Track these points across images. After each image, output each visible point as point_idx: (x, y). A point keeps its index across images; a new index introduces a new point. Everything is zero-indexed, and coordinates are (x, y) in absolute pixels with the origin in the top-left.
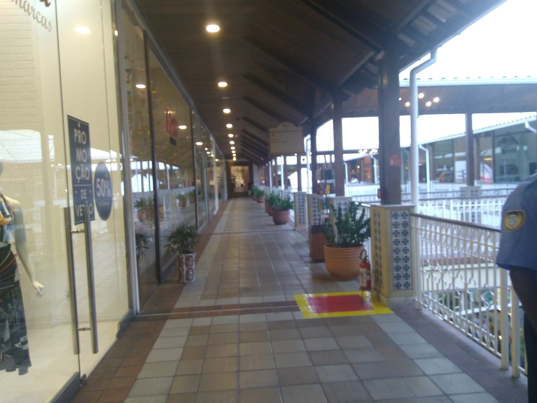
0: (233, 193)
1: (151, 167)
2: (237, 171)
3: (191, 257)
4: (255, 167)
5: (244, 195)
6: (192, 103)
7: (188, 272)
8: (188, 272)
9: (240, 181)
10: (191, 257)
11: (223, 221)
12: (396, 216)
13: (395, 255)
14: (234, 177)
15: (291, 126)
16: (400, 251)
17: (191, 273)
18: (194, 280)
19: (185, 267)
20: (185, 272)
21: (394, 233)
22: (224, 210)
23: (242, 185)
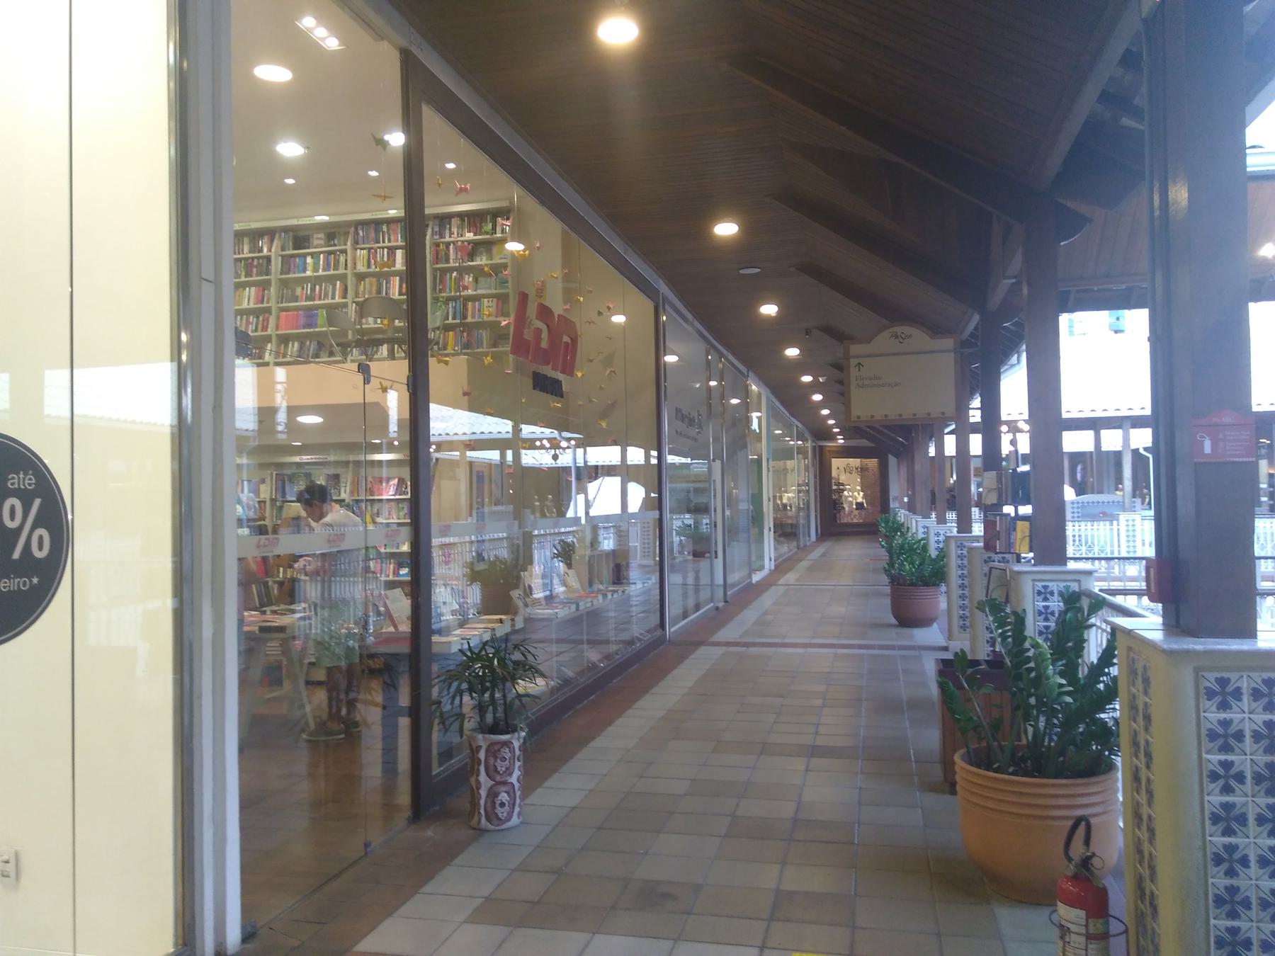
0: (833, 524)
1: (654, 461)
2: (848, 470)
3: (507, 744)
4: (892, 460)
5: (866, 530)
6: (664, 289)
7: (493, 794)
8: (493, 794)
9: (854, 495)
10: (507, 744)
11: (767, 600)
12: (1224, 694)
13: (1219, 881)
14: (839, 484)
15: (918, 338)
16: (1244, 862)
17: (504, 797)
18: (515, 820)
19: (483, 777)
20: (483, 793)
21: (1214, 776)
22: (785, 571)
23: (860, 506)
